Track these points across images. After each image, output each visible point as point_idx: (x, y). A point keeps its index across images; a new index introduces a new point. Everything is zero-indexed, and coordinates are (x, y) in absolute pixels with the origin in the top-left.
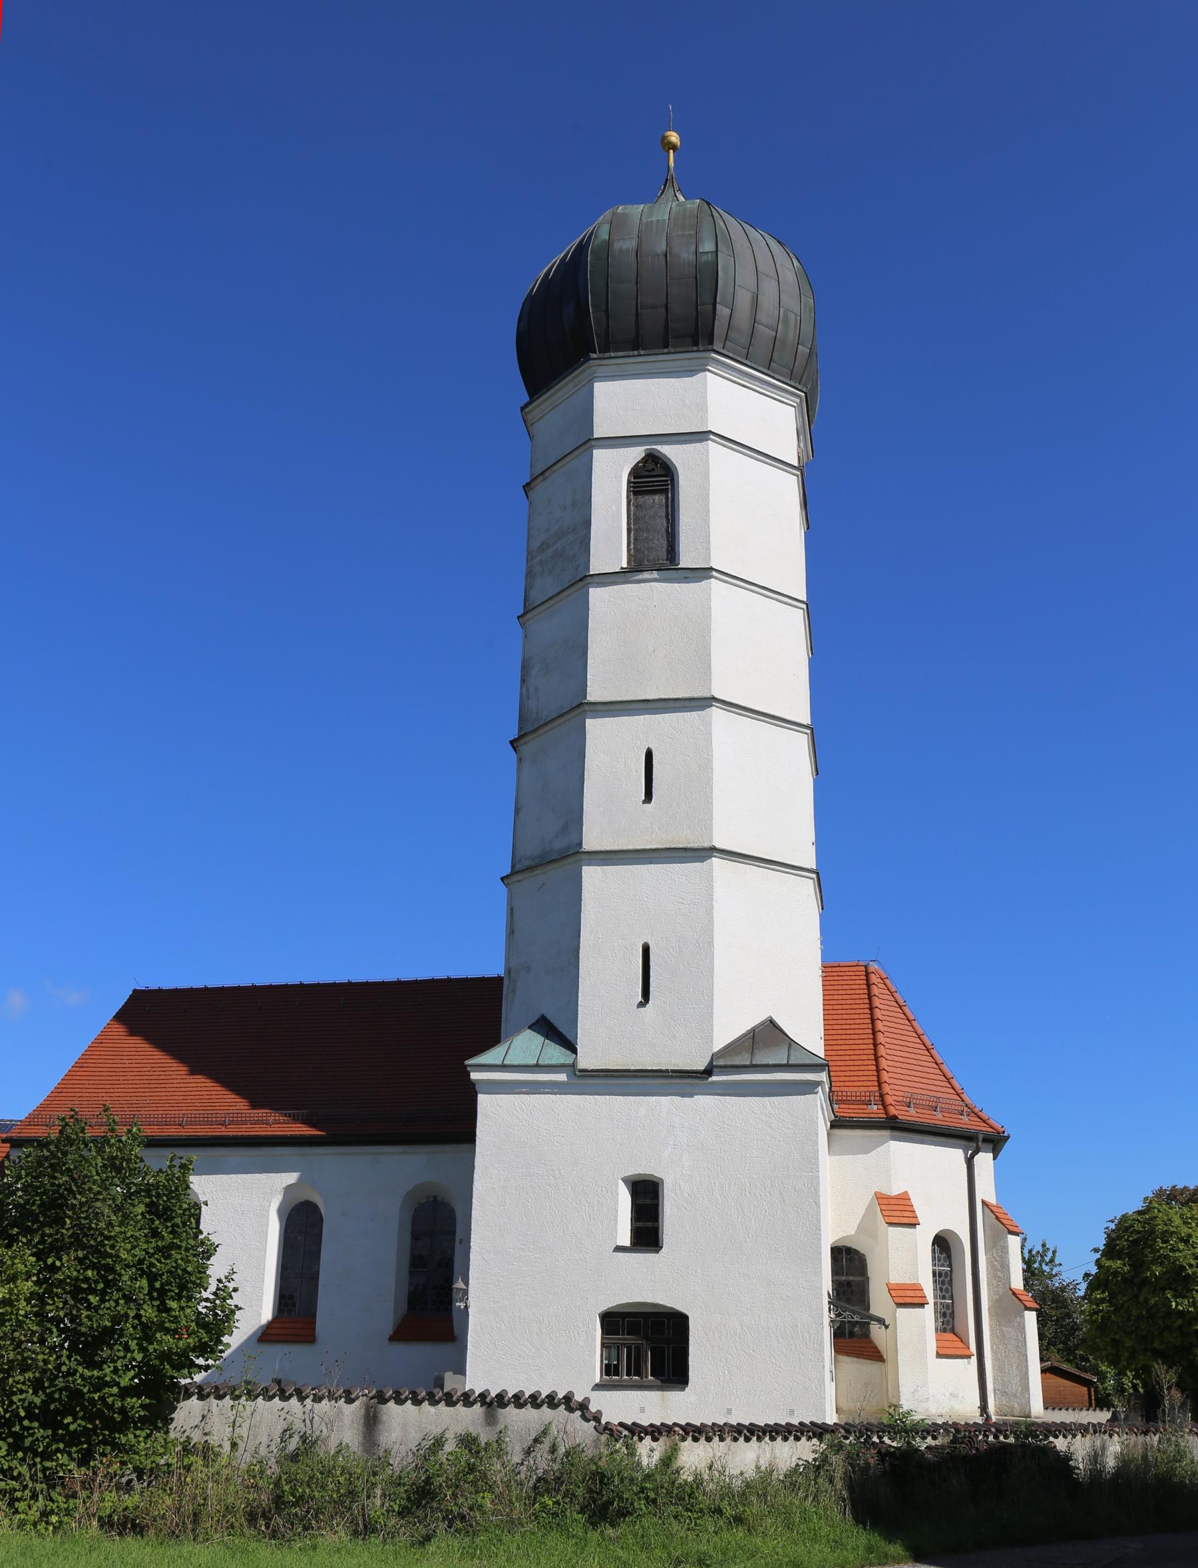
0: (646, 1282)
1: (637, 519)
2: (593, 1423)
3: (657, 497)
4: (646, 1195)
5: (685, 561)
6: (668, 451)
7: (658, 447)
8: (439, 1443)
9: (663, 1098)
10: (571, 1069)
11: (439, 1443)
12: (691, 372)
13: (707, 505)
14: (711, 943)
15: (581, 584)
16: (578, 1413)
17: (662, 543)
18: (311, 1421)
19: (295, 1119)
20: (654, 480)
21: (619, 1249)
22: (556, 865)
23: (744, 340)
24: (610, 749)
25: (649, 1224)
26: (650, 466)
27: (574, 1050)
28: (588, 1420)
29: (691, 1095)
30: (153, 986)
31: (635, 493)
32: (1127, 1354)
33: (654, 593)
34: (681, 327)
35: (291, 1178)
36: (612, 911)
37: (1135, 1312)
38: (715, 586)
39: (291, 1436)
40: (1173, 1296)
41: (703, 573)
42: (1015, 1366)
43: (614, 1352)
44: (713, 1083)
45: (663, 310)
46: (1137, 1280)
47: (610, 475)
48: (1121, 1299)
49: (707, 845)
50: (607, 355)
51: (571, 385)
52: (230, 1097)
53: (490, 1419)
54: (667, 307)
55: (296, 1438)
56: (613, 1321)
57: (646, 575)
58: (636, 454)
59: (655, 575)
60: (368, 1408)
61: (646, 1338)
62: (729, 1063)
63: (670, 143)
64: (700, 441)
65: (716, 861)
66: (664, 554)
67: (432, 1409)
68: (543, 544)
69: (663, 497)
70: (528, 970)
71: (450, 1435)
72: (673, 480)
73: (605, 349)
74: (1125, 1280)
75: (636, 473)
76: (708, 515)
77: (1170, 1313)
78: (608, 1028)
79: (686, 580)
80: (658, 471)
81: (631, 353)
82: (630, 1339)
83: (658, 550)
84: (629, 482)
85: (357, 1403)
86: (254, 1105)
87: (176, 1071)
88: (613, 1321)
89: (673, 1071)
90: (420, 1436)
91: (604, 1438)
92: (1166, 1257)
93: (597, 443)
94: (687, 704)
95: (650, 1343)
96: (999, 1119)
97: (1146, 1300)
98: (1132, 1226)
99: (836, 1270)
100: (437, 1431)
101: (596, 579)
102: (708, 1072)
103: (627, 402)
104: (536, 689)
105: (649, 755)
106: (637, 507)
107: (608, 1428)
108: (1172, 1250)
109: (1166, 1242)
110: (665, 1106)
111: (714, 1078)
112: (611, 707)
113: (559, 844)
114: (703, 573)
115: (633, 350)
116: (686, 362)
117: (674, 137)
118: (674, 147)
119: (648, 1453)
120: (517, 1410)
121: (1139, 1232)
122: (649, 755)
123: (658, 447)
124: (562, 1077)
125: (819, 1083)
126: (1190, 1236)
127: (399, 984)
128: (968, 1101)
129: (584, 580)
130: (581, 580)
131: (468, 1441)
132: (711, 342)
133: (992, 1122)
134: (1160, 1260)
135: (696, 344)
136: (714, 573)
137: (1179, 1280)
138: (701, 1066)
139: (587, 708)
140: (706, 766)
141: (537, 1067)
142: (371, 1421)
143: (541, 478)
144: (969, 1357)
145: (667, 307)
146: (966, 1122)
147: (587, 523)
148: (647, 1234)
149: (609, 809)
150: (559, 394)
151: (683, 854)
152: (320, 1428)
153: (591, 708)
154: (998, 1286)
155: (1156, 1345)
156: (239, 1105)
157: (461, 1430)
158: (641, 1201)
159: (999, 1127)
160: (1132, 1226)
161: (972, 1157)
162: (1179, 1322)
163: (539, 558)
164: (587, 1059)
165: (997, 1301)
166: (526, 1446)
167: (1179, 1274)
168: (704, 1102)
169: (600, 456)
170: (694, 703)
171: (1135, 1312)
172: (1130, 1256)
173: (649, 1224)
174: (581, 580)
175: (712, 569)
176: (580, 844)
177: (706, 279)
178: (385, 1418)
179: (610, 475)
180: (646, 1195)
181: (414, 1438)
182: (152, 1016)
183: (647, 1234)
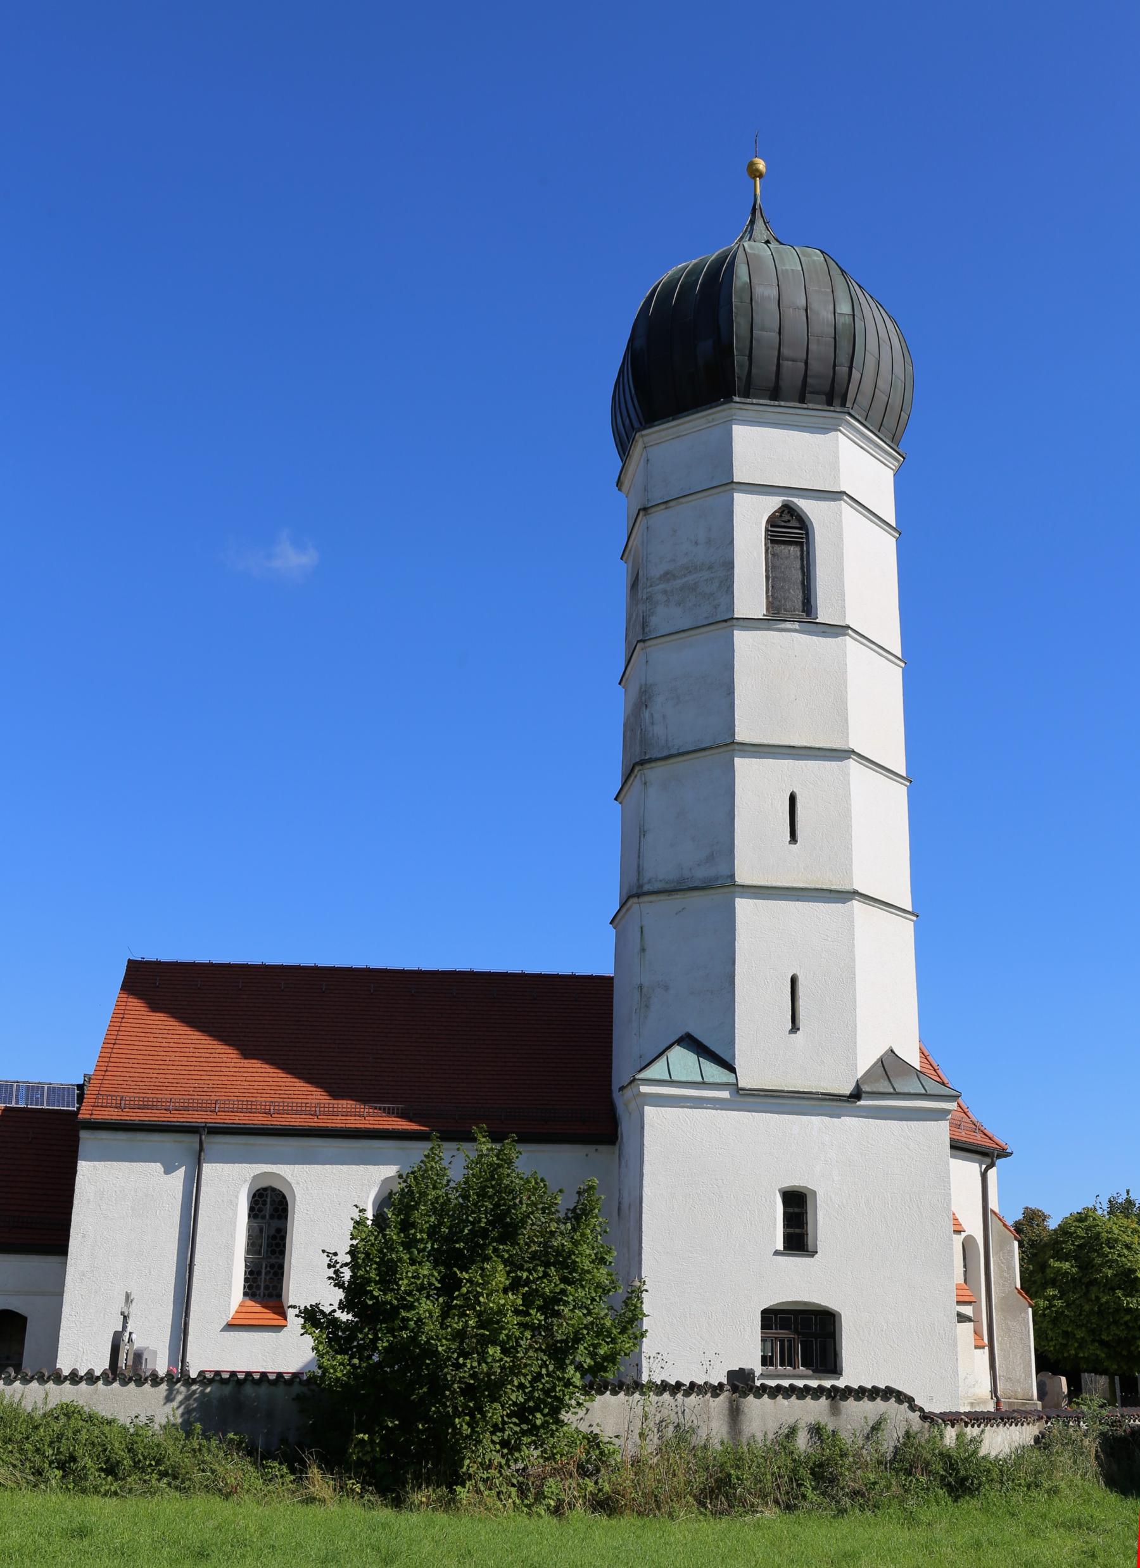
0: (799, 1283)
1: (774, 567)
2: (918, 1413)
3: (792, 548)
4: (796, 1204)
5: (824, 615)
6: (805, 505)
7: (795, 500)
8: (793, 1431)
9: (813, 1118)
10: (737, 1090)
11: (793, 1431)
12: (825, 430)
13: (842, 564)
14: (853, 979)
15: (724, 624)
16: (906, 1404)
17: (797, 595)
18: (683, 1413)
19: (389, 1112)
20: (790, 530)
21: (777, 1253)
22: (701, 893)
23: (866, 405)
24: (757, 788)
25: (798, 1231)
26: (786, 517)
27: (732, 1070)
28: (914, 1411)
29: (839, 1117)
30: (151, 956)
31: (773, 542)
32: (1076, 1345)
33: (790, 644)
34: (820, 389)
35: (391, 1171)
36: (764, 940)
37: (1087, 1308)
38: (849, 643)
39: (666, 1426)
40: (1124, 1295)
41: (839, 630)
42: (1019, 1356)
43: (769, 1344)
44: (858, 1106)
45: (802, 365)
46: (1086, 1280)
47: (750, 519)
48: (1072, 1297)
49: (848, 888)
50: (749, 400)
51: (703, 420)
52: (300, 1085)
53: (835, 1411)
54: (806, 363)
55: (671, 1428)
56: (772, 1318)
57: (788, 625)
58: (773, 503)
59: (796, 626)
60: (731, 1402)
61: (796, 1332)
62: (875, 1090)
63: (757, 170)
64: (834, 500)
65: (855, 903)
66: (799, 606)
67: (785, 1402)
68: (666, 574)
69: (798, 549)
70: (666, 988)
71: (802, 1424)
72: (807, 534)
73: (746, 395)
74: (1073, 1280)
75: (772, 522)
76: (842, 574)
77: (1119, 1309)
78: (763, 1052)
79: (824, 634)
80: (794, 523)
81: (772, 403)
82: (784, 1334)
83: (795, 598)
84: (767, 530)
85: (721, 1397)
86: (334, 1095)
87: (226, 1056)
88: (772, 1318)
89: (823, 1094)
90: (776, 1426)
91: (927, 1425)
92: (1112, 1261)
93: (738, 487)
94: (828, 754)
95: (805, 1336)
96: (1002, 1136)
97: (1098, 1298)
98: (1075, 1232)
99: (254, 1211)
100: (791, 1421)
101: (741, 623)
102: (857, 1095)
103: (766, 450)
104: (664, 717)
105: (793, 799)
106: (774, 555)
107: (926, 1417)
108: (1119, 1255)
109: (1113, 1247)
110: (816, 1124)
111: (862, 1103)
112: (760, 749)
113: (701, 873)
114: (839, 630)
115: (771, 399)
116: (821, 420)
117: (761, 165)
118: (761, 176)
119: (950, 1434)
120: (856, 1403)
121: (1083, 1238)
122: (793, 799)
123: (795, 500)
124: (725, 1094)
125: (949, 1112)
126: (1132, 1243)
127: (419, 973)
128: (974, 1119)
129: (730, 621)
130: (725, 621)
131: (816, 1430)
132: (843, 404)
133: (995, 1139)
134: (1110, 1263)
135: (830, 403)
136: (850, 632)
137: (1127, 1280)
138: (847, 1089)
139: (737, 747)
140: (846, 814)
141: (703, 1084)
142: (735, 1414)
143: (663, 507)
144: (983, 1347)
145: (806, 363)
146: (978, 1139)
147: (730, 565)
148: (797, 1240)
149: (757, 849)
150: (687, 426)
151: (828, 895)
152: (689, 1419)
153: (740, 747)
154: (1004, 1285)
155: (1104, 1337)
156: (316, 1096)
157: (812, 1420)
158: (791, 1210)
159: (1003, 1144)
160: (1075, 1232)
161: (986, 1170)
162: (1127, 1318)
163: (660, 587)
164: (747, 1078)
165: (1003, 1298)
166: (865, 1432)
167: (1128, 1276)
168: (850, 1123)
169: (741, 500)
170: (834, 754)
171: (1087, 1308)
172: (1076, 1258)
173: (798, 1231)
174: (725, 621)
175: (848, 627)
176: (732, 876)
177: (845, 340)
178: (746, 1410)
179: (750, 519)
180: (796, 1204)
181: (772, 1427)
182: (154, 984)
183: (797, 1240)
